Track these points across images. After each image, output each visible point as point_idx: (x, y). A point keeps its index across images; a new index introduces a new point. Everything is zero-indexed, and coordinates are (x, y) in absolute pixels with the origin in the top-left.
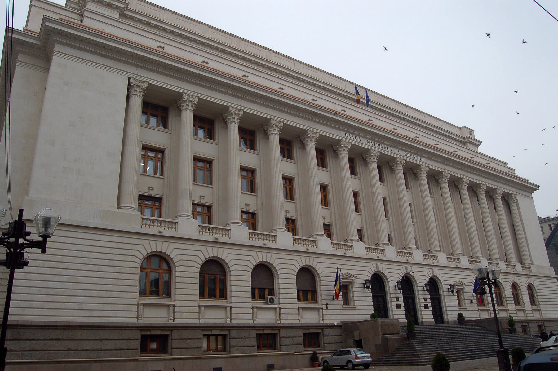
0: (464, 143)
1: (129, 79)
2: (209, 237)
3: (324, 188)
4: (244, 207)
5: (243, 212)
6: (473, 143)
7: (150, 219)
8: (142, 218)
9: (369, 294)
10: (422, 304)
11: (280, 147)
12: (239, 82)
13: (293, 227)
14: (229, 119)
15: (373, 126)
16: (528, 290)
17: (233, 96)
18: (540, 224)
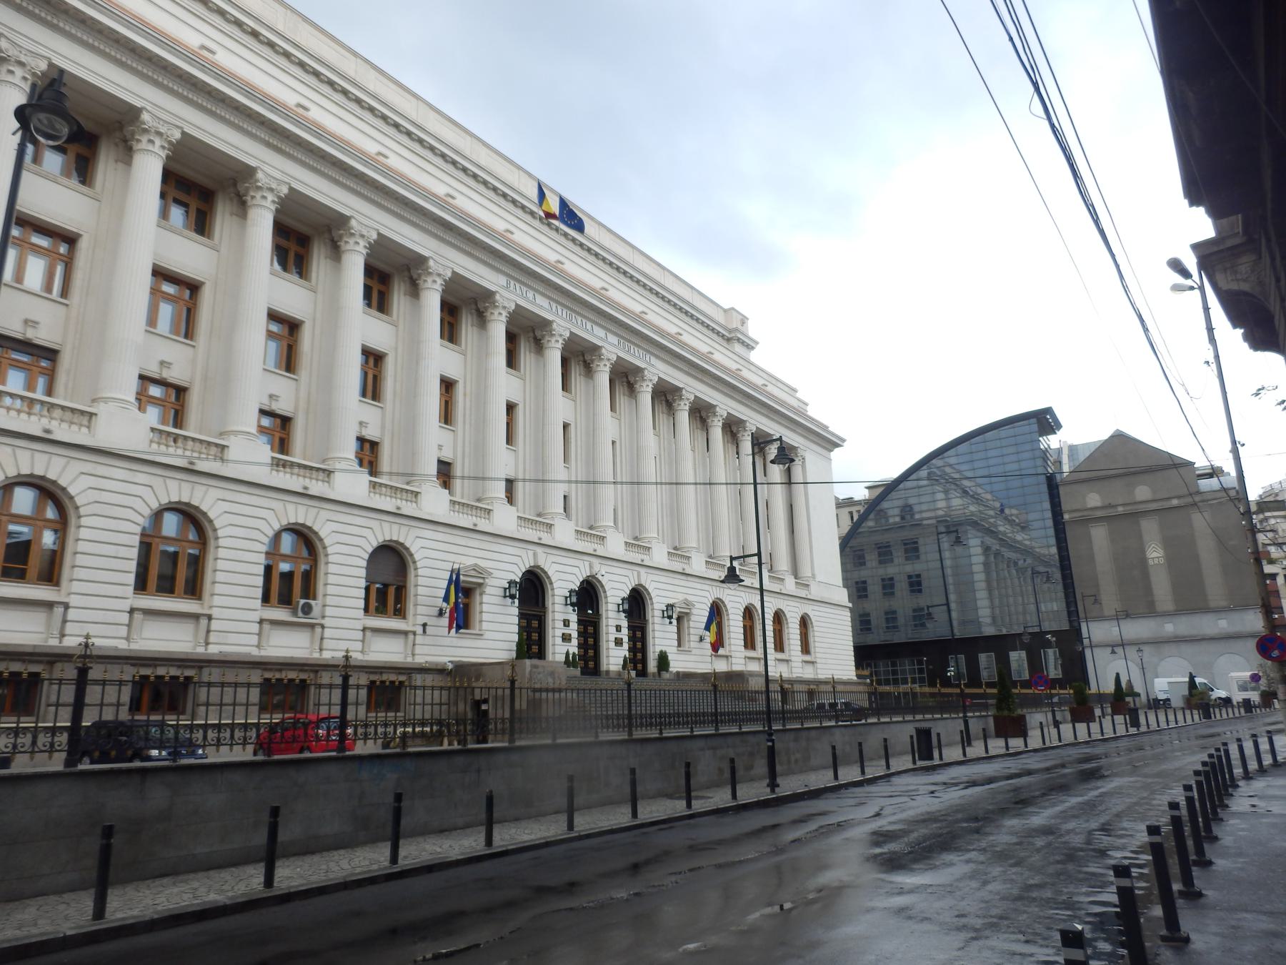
0: (729, 340)
2: (175, 455)
3: (448, 385)
4: (266, 401)
5: (263, 412)
6: (743, 343)
7: (22, 398)
9: (512, 611)
10: (612, 638)
12: (287, 117)
14: (253, 197)
15: (684, 345)
16: (800, 625)
17: (268, 145)
18: (837, 508)
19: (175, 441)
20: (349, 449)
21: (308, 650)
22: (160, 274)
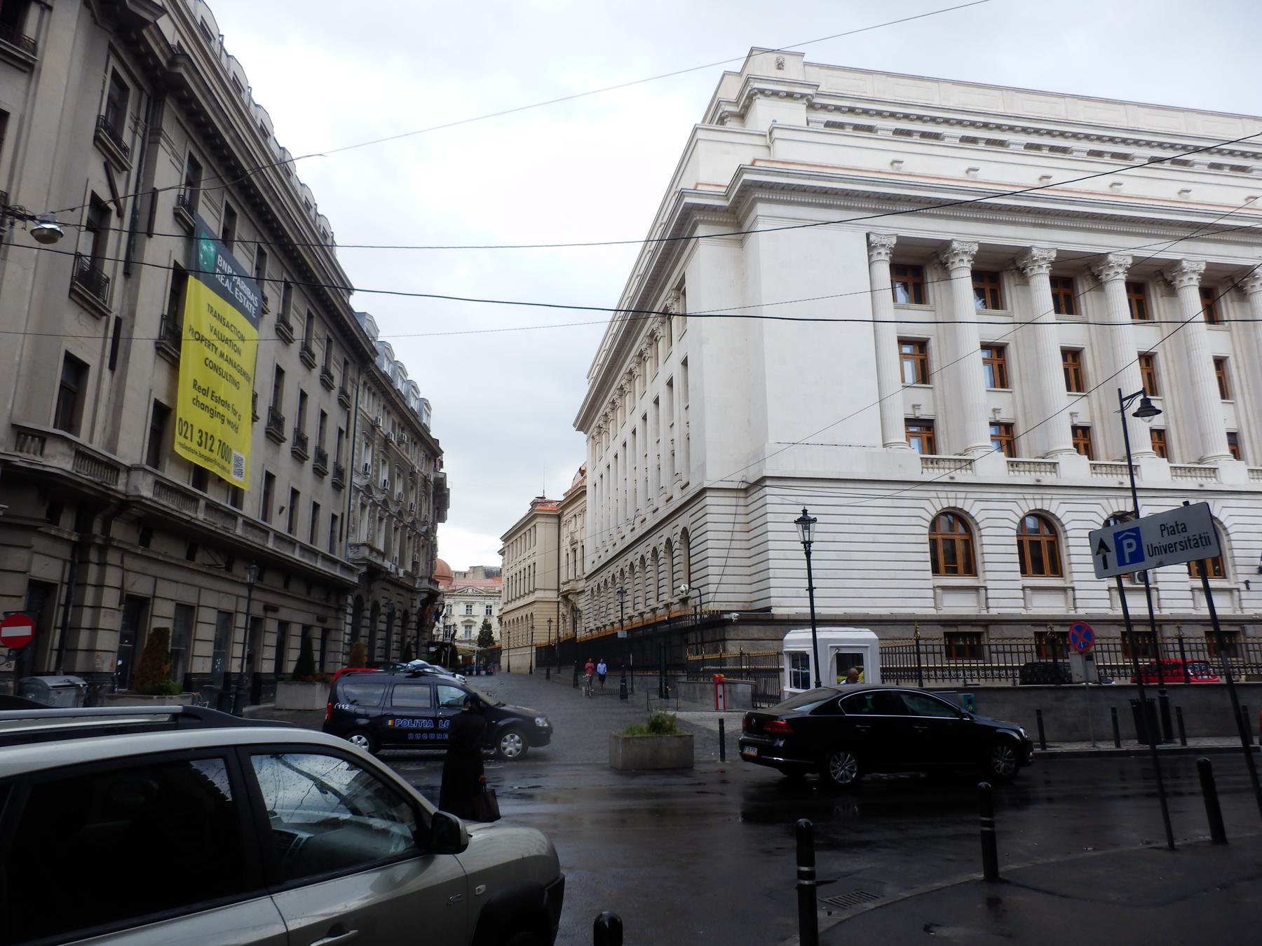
1: (868, 235)
5: (992, 424)
11: (1053, 295)
13: (1162, 445)
17: (1035, 225)
19: (932, 463)
20: (1066, 440)
21: (977, 609)
22: (903, 341)
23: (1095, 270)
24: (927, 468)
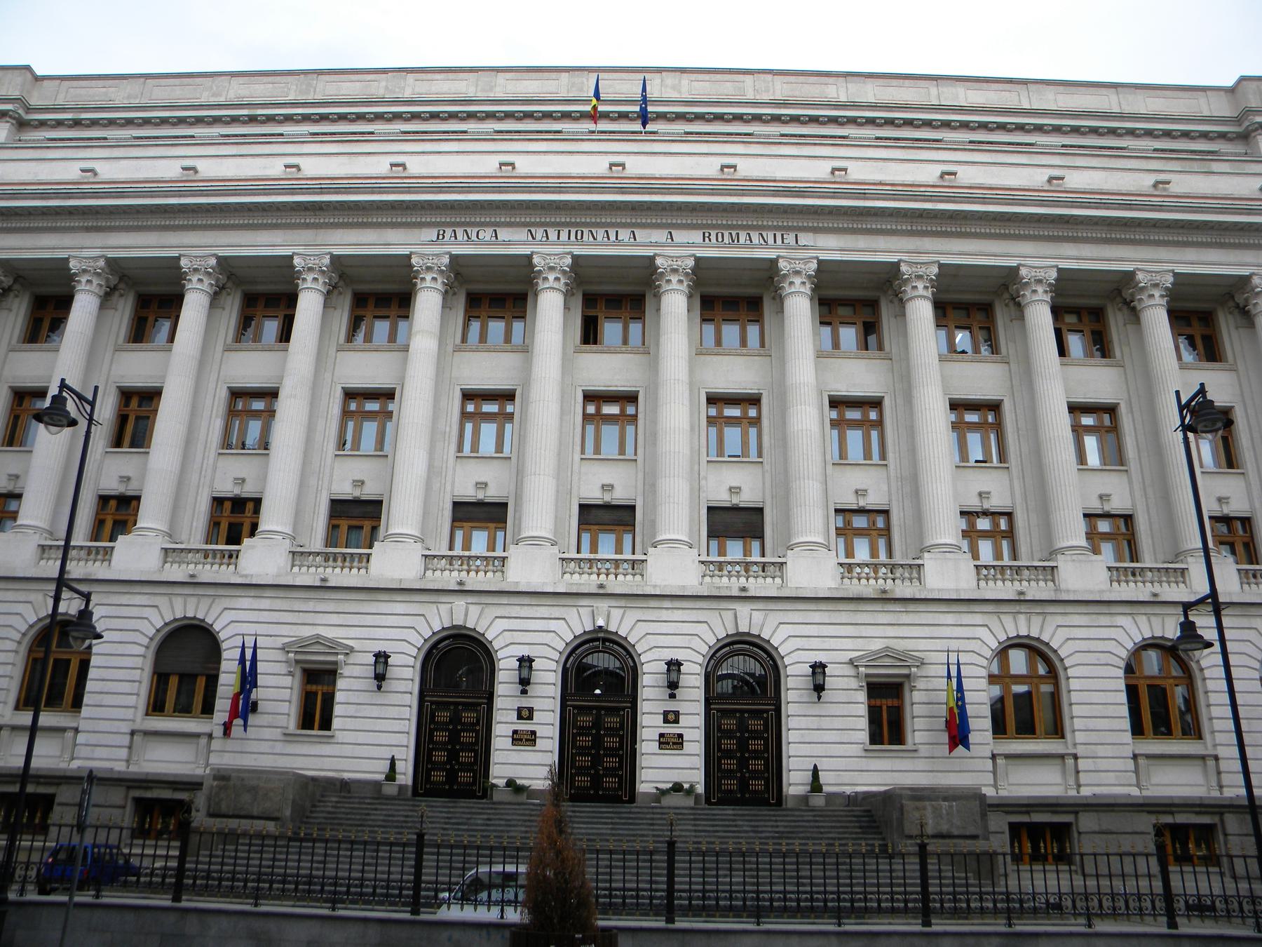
2: (1140, 591)
8: (976, 567)
17: (88, 229)
19: (1134, 574)
22: (1075, 409)
23: (1240, 299)
24: (1249, 584)
